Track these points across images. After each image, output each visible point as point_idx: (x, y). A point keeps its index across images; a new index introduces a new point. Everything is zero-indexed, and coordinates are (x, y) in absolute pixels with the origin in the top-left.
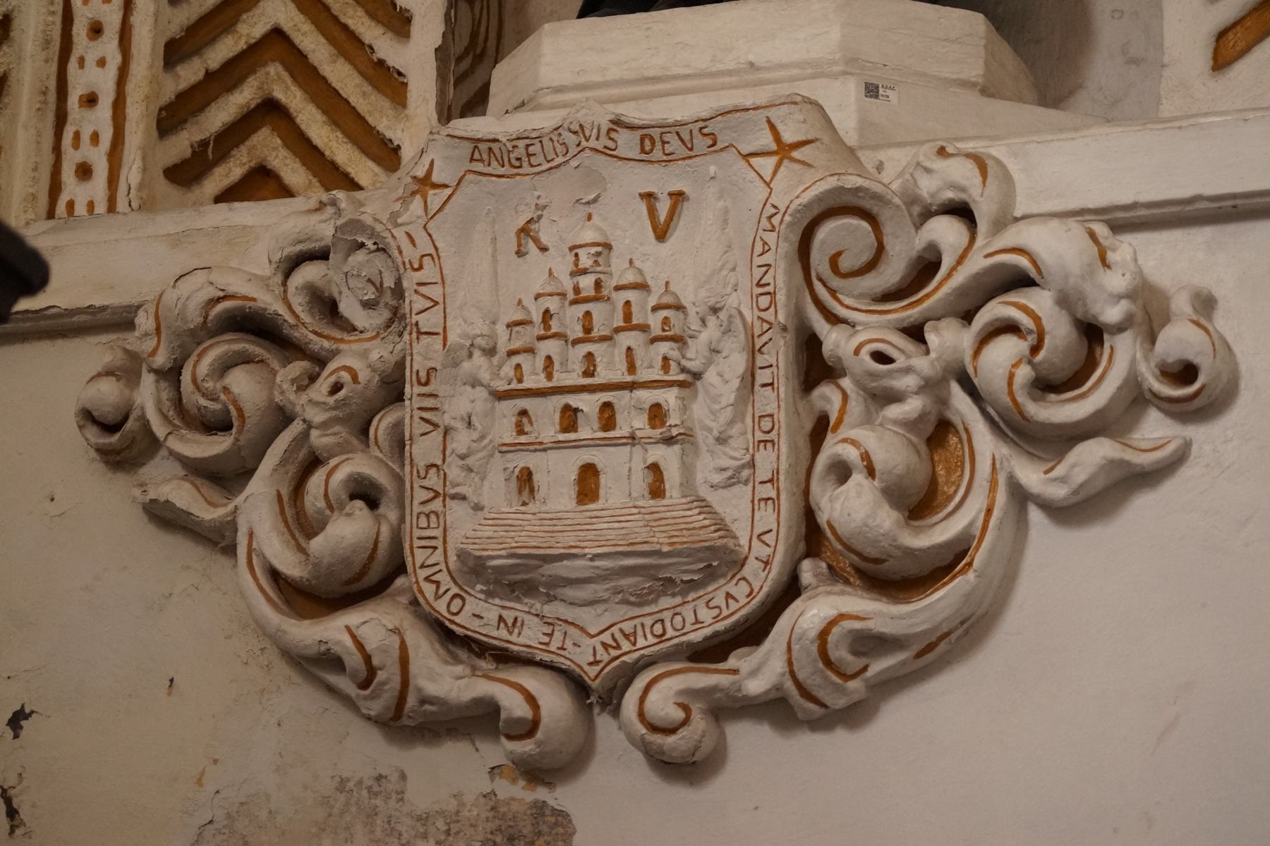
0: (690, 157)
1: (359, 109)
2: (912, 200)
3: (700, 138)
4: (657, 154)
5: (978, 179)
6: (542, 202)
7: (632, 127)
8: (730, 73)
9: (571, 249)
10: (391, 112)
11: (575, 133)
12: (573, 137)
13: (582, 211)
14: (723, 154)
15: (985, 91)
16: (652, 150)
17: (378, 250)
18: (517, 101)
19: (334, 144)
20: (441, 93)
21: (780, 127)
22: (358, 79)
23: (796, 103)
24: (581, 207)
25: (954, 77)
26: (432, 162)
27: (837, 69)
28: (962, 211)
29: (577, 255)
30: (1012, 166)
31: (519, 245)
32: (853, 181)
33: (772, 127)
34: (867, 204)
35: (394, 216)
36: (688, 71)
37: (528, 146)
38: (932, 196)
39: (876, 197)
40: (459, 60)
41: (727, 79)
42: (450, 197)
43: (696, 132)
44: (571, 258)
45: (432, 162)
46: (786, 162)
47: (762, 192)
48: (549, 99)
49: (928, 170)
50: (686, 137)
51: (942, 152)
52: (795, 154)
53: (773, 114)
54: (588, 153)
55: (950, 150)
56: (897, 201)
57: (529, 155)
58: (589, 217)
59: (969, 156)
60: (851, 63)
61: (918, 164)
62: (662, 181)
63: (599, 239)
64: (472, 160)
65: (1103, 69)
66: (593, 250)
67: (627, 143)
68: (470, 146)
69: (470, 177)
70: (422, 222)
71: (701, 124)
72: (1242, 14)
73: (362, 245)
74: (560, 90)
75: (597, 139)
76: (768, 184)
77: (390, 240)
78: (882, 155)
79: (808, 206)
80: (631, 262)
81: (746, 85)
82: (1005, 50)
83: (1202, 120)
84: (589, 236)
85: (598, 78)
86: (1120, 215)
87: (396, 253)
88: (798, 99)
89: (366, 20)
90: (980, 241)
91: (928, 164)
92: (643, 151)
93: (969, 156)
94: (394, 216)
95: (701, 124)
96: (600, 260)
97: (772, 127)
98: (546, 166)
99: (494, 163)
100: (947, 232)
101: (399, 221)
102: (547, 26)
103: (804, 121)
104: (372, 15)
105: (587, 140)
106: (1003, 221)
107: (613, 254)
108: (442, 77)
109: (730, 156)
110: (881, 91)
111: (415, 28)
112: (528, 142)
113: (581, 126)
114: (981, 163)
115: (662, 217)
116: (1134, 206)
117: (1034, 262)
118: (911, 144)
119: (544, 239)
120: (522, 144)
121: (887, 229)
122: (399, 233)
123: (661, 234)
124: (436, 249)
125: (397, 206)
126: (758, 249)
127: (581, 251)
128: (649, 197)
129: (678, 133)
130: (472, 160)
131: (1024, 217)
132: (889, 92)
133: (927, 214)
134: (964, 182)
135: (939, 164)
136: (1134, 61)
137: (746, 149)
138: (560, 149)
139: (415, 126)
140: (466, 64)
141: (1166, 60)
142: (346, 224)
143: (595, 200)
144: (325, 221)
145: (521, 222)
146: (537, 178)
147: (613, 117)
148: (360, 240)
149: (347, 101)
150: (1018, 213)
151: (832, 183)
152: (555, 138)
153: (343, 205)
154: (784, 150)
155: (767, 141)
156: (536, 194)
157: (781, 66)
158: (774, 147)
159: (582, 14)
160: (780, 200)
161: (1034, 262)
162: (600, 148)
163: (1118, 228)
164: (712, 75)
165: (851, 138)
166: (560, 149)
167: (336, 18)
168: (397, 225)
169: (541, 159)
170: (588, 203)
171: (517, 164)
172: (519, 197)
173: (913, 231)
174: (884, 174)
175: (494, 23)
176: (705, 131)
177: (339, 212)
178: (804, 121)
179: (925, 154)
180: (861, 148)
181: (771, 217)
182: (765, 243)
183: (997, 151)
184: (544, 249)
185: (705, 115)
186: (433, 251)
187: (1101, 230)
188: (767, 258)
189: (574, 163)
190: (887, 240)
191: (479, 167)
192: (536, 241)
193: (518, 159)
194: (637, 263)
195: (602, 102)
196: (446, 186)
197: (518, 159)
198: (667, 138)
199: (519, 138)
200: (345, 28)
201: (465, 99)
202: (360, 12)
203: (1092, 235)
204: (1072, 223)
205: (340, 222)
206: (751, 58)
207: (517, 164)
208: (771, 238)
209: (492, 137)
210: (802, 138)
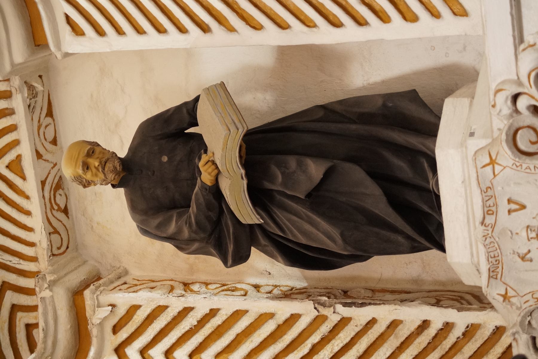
0: (495, 197)
1: (481, 343)
2: (511, 116)
3: (488, 193)
4: (494, 209)
5: (503, 92)
6: (512, 252)
7: (484, 218)
8: (466, 190)
9: (529, 240)
10: (483, 330)
11: (486, 239)
12: (488, 240)
13: (515, 236)
14: (494, 185)
15: (473, 98)
16: (493, 211)
17: (531, 315)
18: (477, 273)
19: (495, 353)
20: (475, 310)
21: (484, 164)
22: (470, 344)
23: (475, 159)
24: (514, 236)
25: (468, 108)
26: (498, 294)
27: (464, 149)
28: (515, 98)
29: (531, 238)
30: (499, 80)
31: (528, 260)
32: (504, 137)
33: (484, 166)
34: (512, 132)
35: (518, 308)
36: (465, 206)
37: (491, 257)
38: (509, 109)
39: (509, 128)
40: (462, 304)
41: (468, 191)
42: (510, 287)
43: (486, 194)
44: (532, 241)
45: (498, 294)
46: (497, 161)
47: (507, 170)
48: (476, 259)
49: (500, 111)
50: (488, 198)
51: (494, 106)
52: (494, 158)
53: (480, 165)
54: (494, 234)
55: (493, 103)
56: (511, 121)
57: (495, 257)
58: (517, 234)
59: (495, 96)
60: (463, 145)
61: (498, 114)
62: (503, 207)
63: (525, 229)
64: (496, 278)
65: (467, 59)
66: (529, 232)
67: (490, 220)
68: (491, 279)
69: (503, 279)
70: (520, 298)
71: (483, 192)
72: (447, 6)
73: (529, 322)
74: (472, 255)
75: (488, 230)
76: (505, 168)
77: (527, 310)
78: (495, 129)
79: (513, 152)
80: (534, 218)
81: (470, 183)
82: (458, 92)
83: (483, 14)
84: (524, 234)
85: (468, 240)
86: (517, 41)
87: (532, 307)
88: (474, 158)
89: (447, 340)
90: (526, 91)
91: (498, 111)
92: (493, 214)
93: (495, 96)
94: (518, 308)
95: (483, 192)
96: (533, 229)
97: (484, 166)
98: (498, 250)
99: (498, 270)
100: (523, 103)
101: (519, 306)
102: (449, 260)
103: (482, 155)
104: (445, 338)
105: (488, 234)
106: (519, 83)
107: (531, 225)
108: (469, 310)
109: (495, 182)
110: (472, 131)
111: (450, 320)
112: (489, 257)
113: (484, 236)
114: (498, 91)
115: (517, 207)
116: (514, 36)
117: (533, 70)
118: (491, 117)
119: (525, 251)
120: (490, 260)
121: (521, 124)
122: (524, 306)
123: (523, 207)
124: (530, 293)
125: (514, 307)
126: (528, 171)
127: (530, 236)
128: (510, 212)
129: (486, 201)
130: (496, 278)
131: (518, 76)
132: (473, 128)
133: (517, 111)
134: (505, 97)
135: (498, 107)
136: (465, 48)
137: (492, 176)
138: (492, 245)
139: (488, 320)
140: (462, 301)
141: (463, 34)
142: (522, 328)
143: (511, 232)
144: (521, 338)
145: (519, 260)
146: (503, 254)
147: (480, 225)
148: (527, 323)
149: (479, 348)
150: (516, 78)
151: (504, 144)
152: (488, 247)
153: (514, 330)
154: (492, 162)
155: (489, 169)
156: (509, 254)
157: (463, 171)
158: (491, 166)
159: (442, 249)
160: (510, 163)
161: (533, 70)
162: (492, 229)
163: (522, 41)
164: (466, 197)
165: (489, 141)
166: (492, 245)
167: (447, 353)
168: (521, 307)
169: (496, 253)
170: (512, 234)
171: (498, 262)
172: (510, 260)
173: (522, 116)
174: (502, 128)
175: (449, 293)
176: (485, 191)
177: (517, 332)
178: (482, 155)
179: (494, 112)
180: (492, 137)
181: (517, 167)
182: (526, 168)
183: (493, 87)
184: (529, 251)
185: (479, 191)
186: (531, 294)
187: (522, 47)
188: (532, 168)
189: (497, 239)
190: (526, 124)
191: (499, 276)
192: (526, 254)
193: (496, 261)
194: (534, 216)
195: (475, 228)
196: (506, 289)
197: (496, 261)
198: (488, 205)
199: (488, 261)
200: (450, 349)
201: (477, 303)
202: (444, 342)
203: (524, 50)
204: (519, 57)
205: (521, 332)
206: (460, 183)
207: (498, 262)
208: (524, 166)
209: (488, 271)
210: (488, 156)
